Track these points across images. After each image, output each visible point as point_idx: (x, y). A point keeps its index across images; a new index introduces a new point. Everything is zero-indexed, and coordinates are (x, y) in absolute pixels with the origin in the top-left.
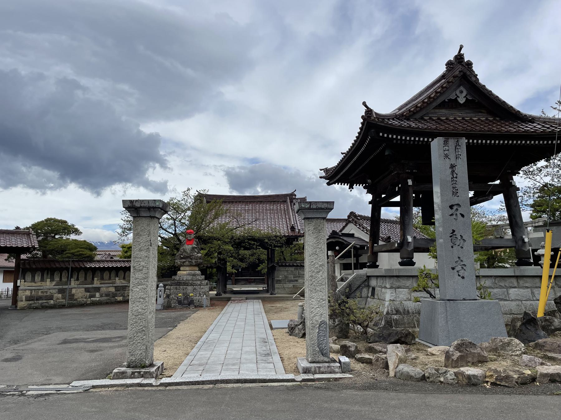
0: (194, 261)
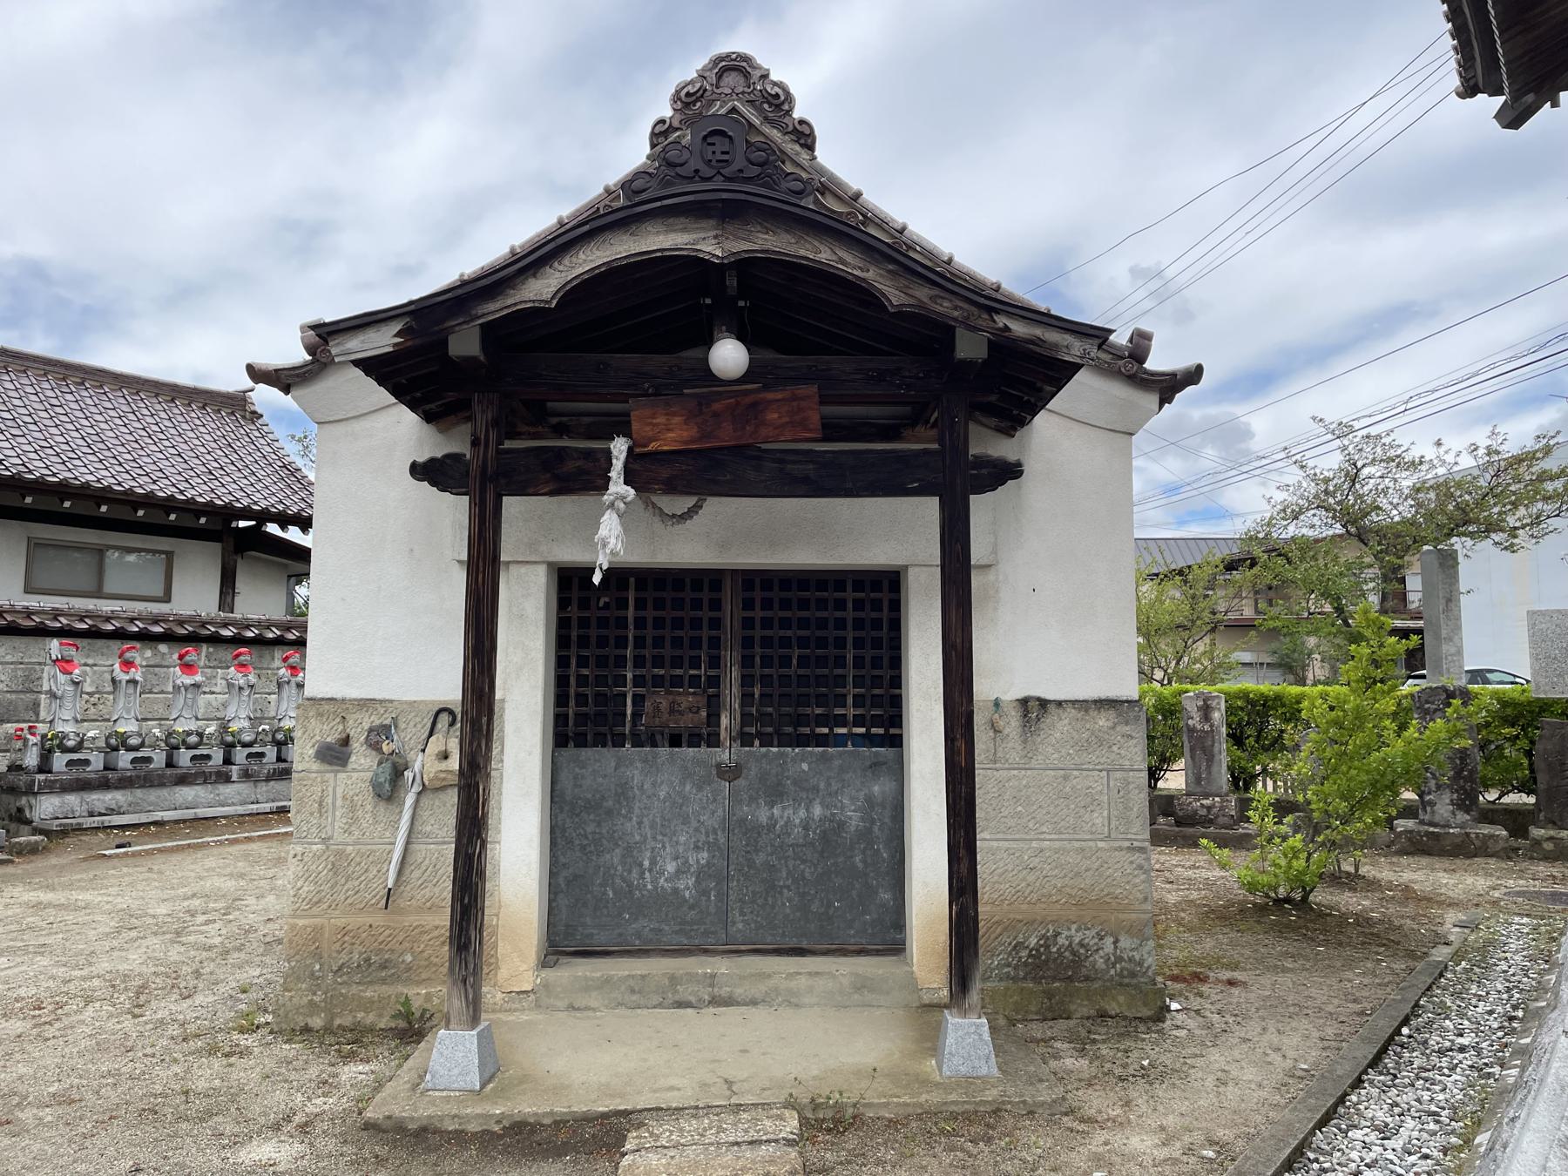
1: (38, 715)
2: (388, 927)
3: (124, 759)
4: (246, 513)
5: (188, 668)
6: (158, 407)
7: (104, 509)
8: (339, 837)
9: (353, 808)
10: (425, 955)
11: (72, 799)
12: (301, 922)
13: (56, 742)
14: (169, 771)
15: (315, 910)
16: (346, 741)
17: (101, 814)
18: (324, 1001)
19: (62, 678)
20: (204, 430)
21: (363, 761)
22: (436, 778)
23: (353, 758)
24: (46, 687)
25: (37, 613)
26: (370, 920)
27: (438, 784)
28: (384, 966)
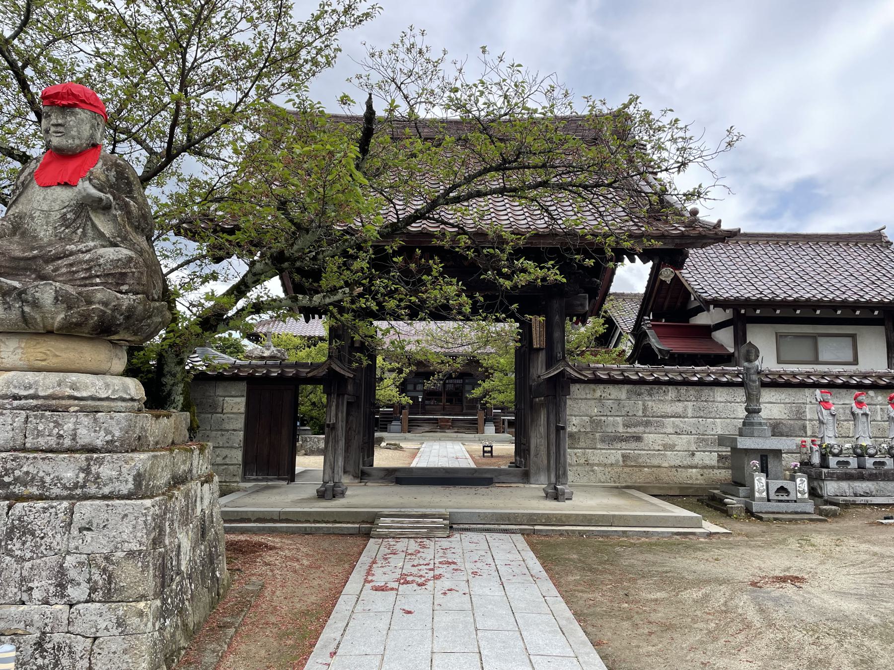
0: (46, 294)
1: (806, 433)
6: (831, 249)
7: (858, 313)
11: (844, 485)
13: (828, 450)
17: (861, 496)
20: (859, 259)
24: (808, 417)
25: (800, 374)
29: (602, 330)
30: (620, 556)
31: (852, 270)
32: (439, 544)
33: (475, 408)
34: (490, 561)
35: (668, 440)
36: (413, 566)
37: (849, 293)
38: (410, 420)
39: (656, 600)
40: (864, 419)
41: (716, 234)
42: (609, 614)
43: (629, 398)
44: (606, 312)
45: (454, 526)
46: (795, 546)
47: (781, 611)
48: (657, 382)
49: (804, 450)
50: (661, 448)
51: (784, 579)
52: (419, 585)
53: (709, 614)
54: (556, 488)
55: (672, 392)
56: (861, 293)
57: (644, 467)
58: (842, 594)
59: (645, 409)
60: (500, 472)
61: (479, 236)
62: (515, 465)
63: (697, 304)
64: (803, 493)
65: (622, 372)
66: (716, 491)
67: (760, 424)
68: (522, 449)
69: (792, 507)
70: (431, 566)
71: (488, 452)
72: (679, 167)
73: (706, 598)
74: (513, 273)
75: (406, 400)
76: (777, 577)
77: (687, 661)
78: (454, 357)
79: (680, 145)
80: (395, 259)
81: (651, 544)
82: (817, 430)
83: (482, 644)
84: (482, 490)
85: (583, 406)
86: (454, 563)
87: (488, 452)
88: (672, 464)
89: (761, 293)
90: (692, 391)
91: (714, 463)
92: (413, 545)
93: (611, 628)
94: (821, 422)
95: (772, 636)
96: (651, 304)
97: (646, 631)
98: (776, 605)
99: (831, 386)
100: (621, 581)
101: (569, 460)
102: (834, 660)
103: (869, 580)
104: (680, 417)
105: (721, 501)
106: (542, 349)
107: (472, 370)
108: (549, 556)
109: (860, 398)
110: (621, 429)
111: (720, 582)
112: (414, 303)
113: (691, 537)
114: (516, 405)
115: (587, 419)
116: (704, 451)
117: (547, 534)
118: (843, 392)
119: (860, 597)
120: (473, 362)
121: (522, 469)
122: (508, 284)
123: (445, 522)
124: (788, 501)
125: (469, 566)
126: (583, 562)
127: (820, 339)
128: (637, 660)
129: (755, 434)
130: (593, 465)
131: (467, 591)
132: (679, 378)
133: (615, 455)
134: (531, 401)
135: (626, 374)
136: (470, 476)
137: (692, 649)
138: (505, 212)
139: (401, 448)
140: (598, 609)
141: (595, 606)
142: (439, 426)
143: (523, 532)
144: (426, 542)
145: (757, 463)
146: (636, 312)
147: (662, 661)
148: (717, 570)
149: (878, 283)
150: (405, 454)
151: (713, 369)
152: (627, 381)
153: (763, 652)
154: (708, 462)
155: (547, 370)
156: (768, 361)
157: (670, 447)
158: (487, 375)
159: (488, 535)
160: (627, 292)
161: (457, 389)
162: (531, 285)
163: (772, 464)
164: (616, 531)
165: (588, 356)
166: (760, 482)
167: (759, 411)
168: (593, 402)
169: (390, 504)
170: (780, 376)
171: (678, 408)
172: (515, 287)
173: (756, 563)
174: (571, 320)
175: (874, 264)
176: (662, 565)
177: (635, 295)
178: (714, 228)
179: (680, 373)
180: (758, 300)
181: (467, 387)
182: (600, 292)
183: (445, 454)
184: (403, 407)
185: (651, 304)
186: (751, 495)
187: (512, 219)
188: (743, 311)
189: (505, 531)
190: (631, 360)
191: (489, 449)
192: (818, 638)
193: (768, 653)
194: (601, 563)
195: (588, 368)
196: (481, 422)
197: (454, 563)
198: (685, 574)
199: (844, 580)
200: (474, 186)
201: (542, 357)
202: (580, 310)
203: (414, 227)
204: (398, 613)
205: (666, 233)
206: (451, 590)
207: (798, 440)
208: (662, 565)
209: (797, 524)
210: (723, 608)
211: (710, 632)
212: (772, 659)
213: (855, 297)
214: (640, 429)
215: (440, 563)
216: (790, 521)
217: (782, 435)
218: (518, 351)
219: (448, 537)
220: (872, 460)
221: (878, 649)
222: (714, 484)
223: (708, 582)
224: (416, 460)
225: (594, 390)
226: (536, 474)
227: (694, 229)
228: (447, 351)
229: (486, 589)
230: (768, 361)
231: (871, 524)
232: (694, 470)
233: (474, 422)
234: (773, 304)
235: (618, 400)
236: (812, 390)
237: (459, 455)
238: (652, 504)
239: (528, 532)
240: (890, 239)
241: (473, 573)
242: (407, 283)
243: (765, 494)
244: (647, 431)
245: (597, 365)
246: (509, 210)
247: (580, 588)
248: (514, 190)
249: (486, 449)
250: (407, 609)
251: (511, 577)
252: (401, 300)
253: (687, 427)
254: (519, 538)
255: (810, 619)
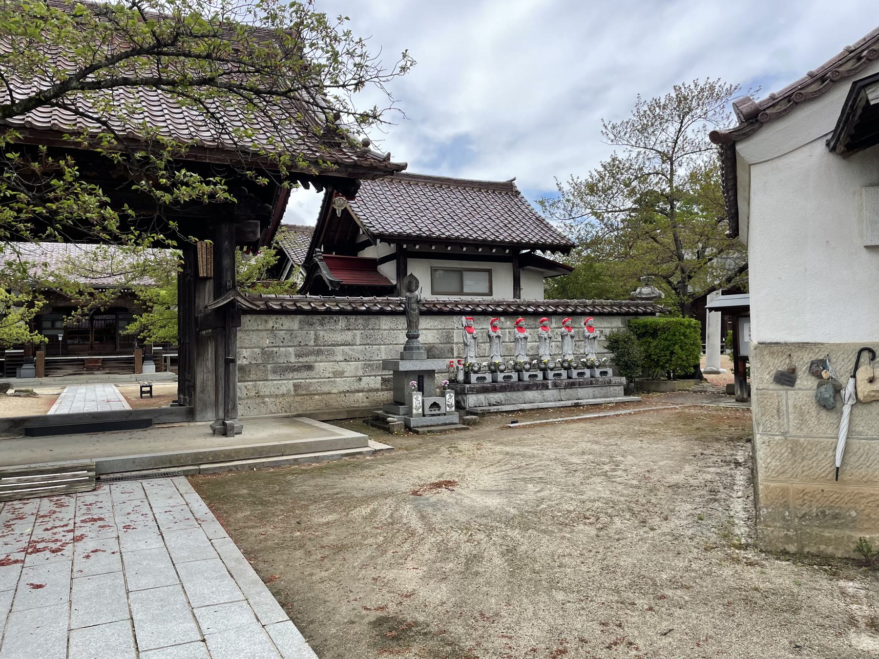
2: (836, 492)
3: (500, 377)
4: (527, 245)
5: (520, 329)
8: (793, 431)
9: (802, 414)
10: (866, 512)
11: (482, 397)
12: (772, 485)
14: (521, 383)
15: (781, 477)
16: (793, 371)
17: (494, 405)
18: (796, 535)
19: (469, 336)
20: (495, 204)
21: (806, 382)
22: (868, 395)
23: (798, 382)
24: (455, 341)
25: (450, 303)
26: (822, 487)
27: (869, 399)
28: (835, 517)
29: (273, 261)
30: (292, 484)
31: (490, 214)
32: (82, 499)
33: (132, 346)
34: (147, 510)
35: (338, 367)
36: (47, 530)
37: (488, 233)
38: (47, 363)
39: (328, 523)
40: (497, 341)
41: (386, 166)
42: (281, 546)
43: (301, 329)
44: (277, 243)
45: (102, 477)
46: (446, 453)
47: (439, 515)
48: (329, 312)
49: (452, 369)
50: (331, 375)
51: (438, 485)
52: (53, 552)
53: (378, 528)
54: (224, 424)
55: (342, 322)
56: (497, 234)
57: (315, 394)
58: (486, 492)
59: (316, 338)
60: (160, 412)
61: (129, 142)
62: (178, 403)
63: (365, 238)
64: (450, 406)
65: (295, 302)
66: (379, 412)
67: (418, 348)
68: (186, 386)
69: (442, 419)
70: (71, 527)
71: (147, 393)
72: (356, 85)
73: (374, 512)
74: (174, 185)
75: (38, 338)
76: (433, 484)
77: (359, 579)
78: (102, 289)
79: (357, 60)
80: (9, 155)
81: (322, 468)
82: (462, 352)
83: (134, 608)
84: (139, 433)
85: (254, 337)
86: (101, 519)
87: (147, 393)
88: (341, 389)
89: (420, 230)
90: (361, 320)
91: (378, 386)
92: (46, 505)
93: (283, 560)
94: (466, 345)
95: (433, 540)
96: (322, 237)
97: (319, 557)
98: (434, 510)
99: (473, 313)
100: (293, 510)
101: (239, 394)
102: (486, 554)
103: (506, 477)
104: (349, 345)
105: (384, 420)
106: (210, 278)
107: (128, 302)
108: (216, 495)
109: (495, 323)
110: (293, 359)
111: (385, 495)
112: (40, 214)
113: (358, 456)
114: (179, 340)
115: (258, 350)
116: (370, 376)
117: (214, 472)
118: (482, 318)
119: (500, 492)
120: (127, 295)
121: (186, 406)
122: (167, 198)
123: (91, 474)
124: (439, 415)
125: (121, 520)
126: (254, 496)
127: (466, 275)
128: (311, 589)
129: (414, 357)
130: (263, 397)
131: (116, 549)
132: (349, 308)
133: (286, 385)
134: (198, 333)
135: (298, 305)
136: (124, 419)
137: (364, 566)
138: (162, 119)
139: (35, 394)
140: (270, 543)
141: (266, 540)
142: (85, 368)
143: (186, 474)
144: (65, 499)
145: (415, 383)
146: (308, 245)
147: (335, 584)
148: (383, 485)
149: (509, 226)
150: (40, 401)
151: (379, 299)
152: (299, 312)
153: (427, 556)
154: (372, 386)
155: (215, 300)
156: (424, 293)
157: (339, 374)
158: (146, 307)
159: (145, 482)
160: (298, 224)
161: (107, 325)
162: (195, 202)
163: (427, 382)
164: (287, 460)
165: (259, 288)
166: (417, 399)
167: (417, 337)
168: (265, 334)
169: (16, 460)
170: (434, 306)
171: (348, 336)
172: (176, 202)
173: (416, 473)
174: (241, 249)
175: (506, 209)
176: (333, 487)
177: (307, 228)
178: (384, 160)
179: (350, 303)
180: (417, 236)
181: (121, 323)
182: (273, 220)
183: (93, 397)
184: (37, 347)
185: (322, 237)
186: (409, 413)
187: (171, 127)
188: (405, 246)
189: (166, 475)
190: (302, 291)
191: (148, 389)
192: (471, 535)
193: (431, 557)
194: (271, 495)
195: (260, 298)
196: (138, 360)
197: (101, 519)
198: (355, 493)
199: (487, 478)
200: (122, 70)
201: (209, 286)
202: (251, 238)
203: (39, 117)
204: (24, 588)
205: (340, 161)
206: (96, 551)
207: (447, 361)
208: (333, 487)
209: (446, 434)
210: (390, 520)
211: (379, 546)
212: (435, 562)
213: (493, 237)
214: (312, 358)
215: (83, 521)
216: (441, 431)
217: (434, 358)
218: (180, 276)
219: (94, 490)
220: (502, 375)
221: (519, 537)
222: (377, 405)
223: (375, 497)
224: (55, 407)
225: (266, 321)
226: (202, 410)
227: (366, 159)
228: (94, 281)
229: (142, 544)
230: (424, 293)
231: (502, 428)
232: (361, 394)
233: (131, 361)
234: (429, 240)
235: (290, 331)
236: (459, 317)
237: (111, 397)
238: (322, 429)
239: (193, 473)
240: (519, 189)
241: (124, 527)
242: (30, 189)
243: (421, 410)
244: (319, 359)
245: (269, 296)
246: (167, 117)
247: (250, 524)
248: (173, 83)
249: (144, 389)
250: (36, 582)
251: (172, 525)
252: (19, 211)
253: (352, 356)
254: (182, 481)
255: (463, 518)
